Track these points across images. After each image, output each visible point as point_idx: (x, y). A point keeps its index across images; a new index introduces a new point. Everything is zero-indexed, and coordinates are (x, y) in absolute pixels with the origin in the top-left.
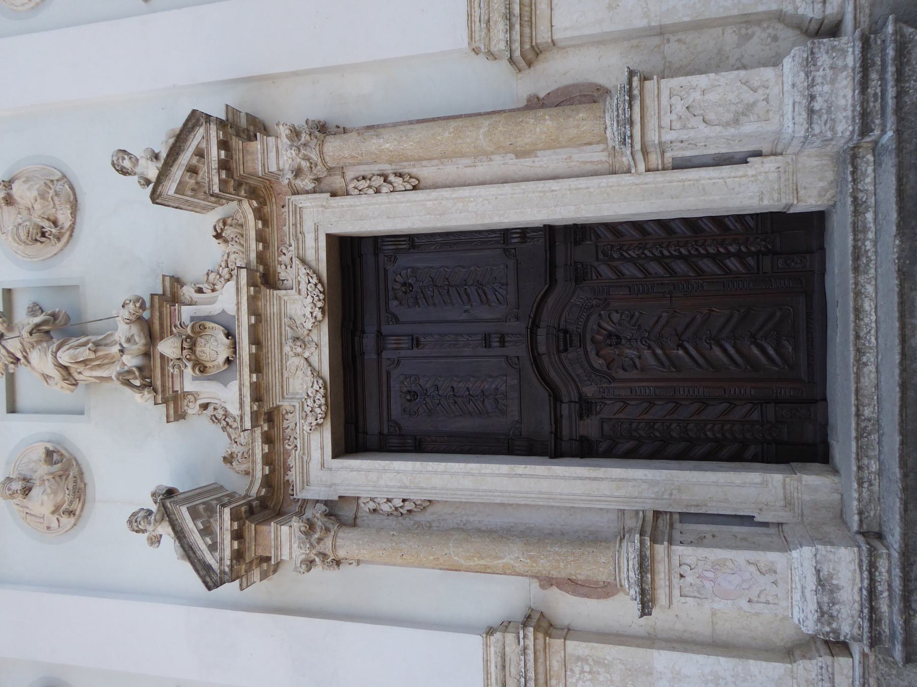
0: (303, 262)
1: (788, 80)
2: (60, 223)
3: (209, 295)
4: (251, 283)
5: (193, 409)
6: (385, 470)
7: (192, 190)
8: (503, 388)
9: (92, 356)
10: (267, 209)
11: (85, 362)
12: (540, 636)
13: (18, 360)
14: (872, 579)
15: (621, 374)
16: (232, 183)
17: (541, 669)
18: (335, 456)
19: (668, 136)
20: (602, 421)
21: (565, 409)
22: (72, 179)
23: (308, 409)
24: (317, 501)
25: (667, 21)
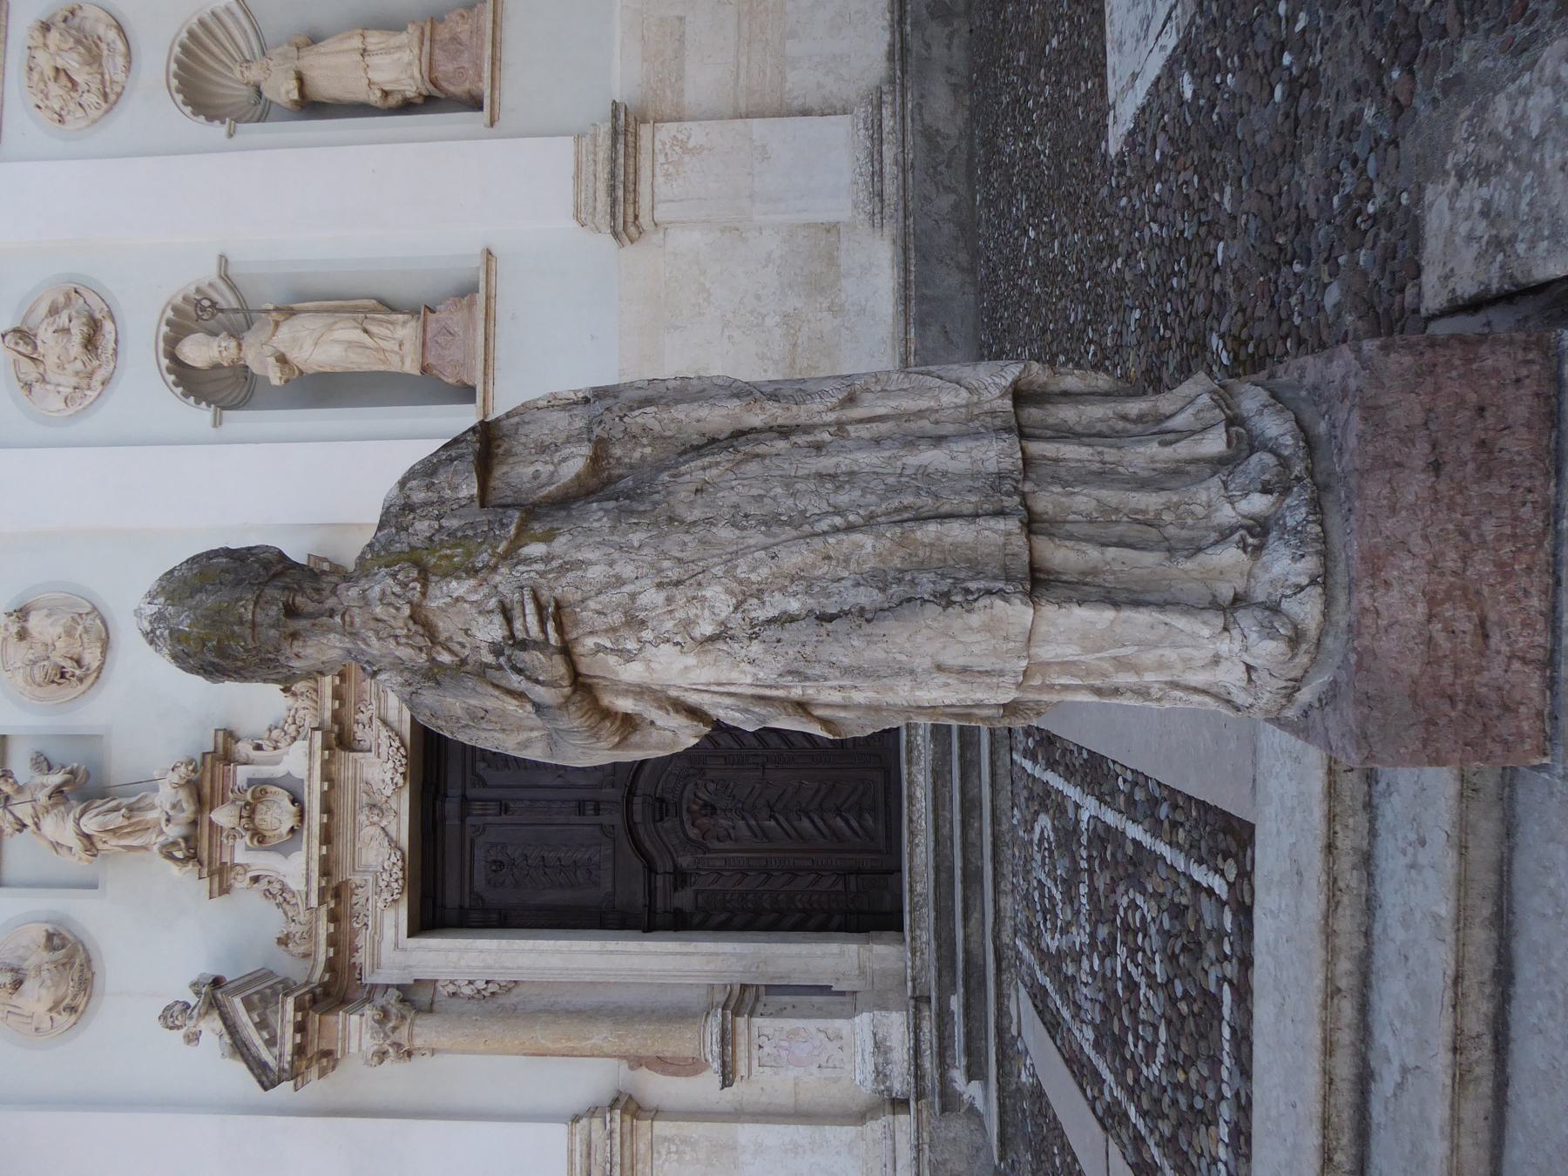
0: (385, 722)
3: (268, 753)
4: (326, 746)
5: (241, 882)
6: (467, 950)
8: (596, 859)
11: (114, 831)
12: (627, 1118)
13: (25, 826)
14: (917, 1040)
15: (716, 845)
17: (627, 1154)
18: (411, 934)
20: (697, 893)
21: (660, 881)
22: (106, 616)
23: (383, 884)
24: (388, 986)
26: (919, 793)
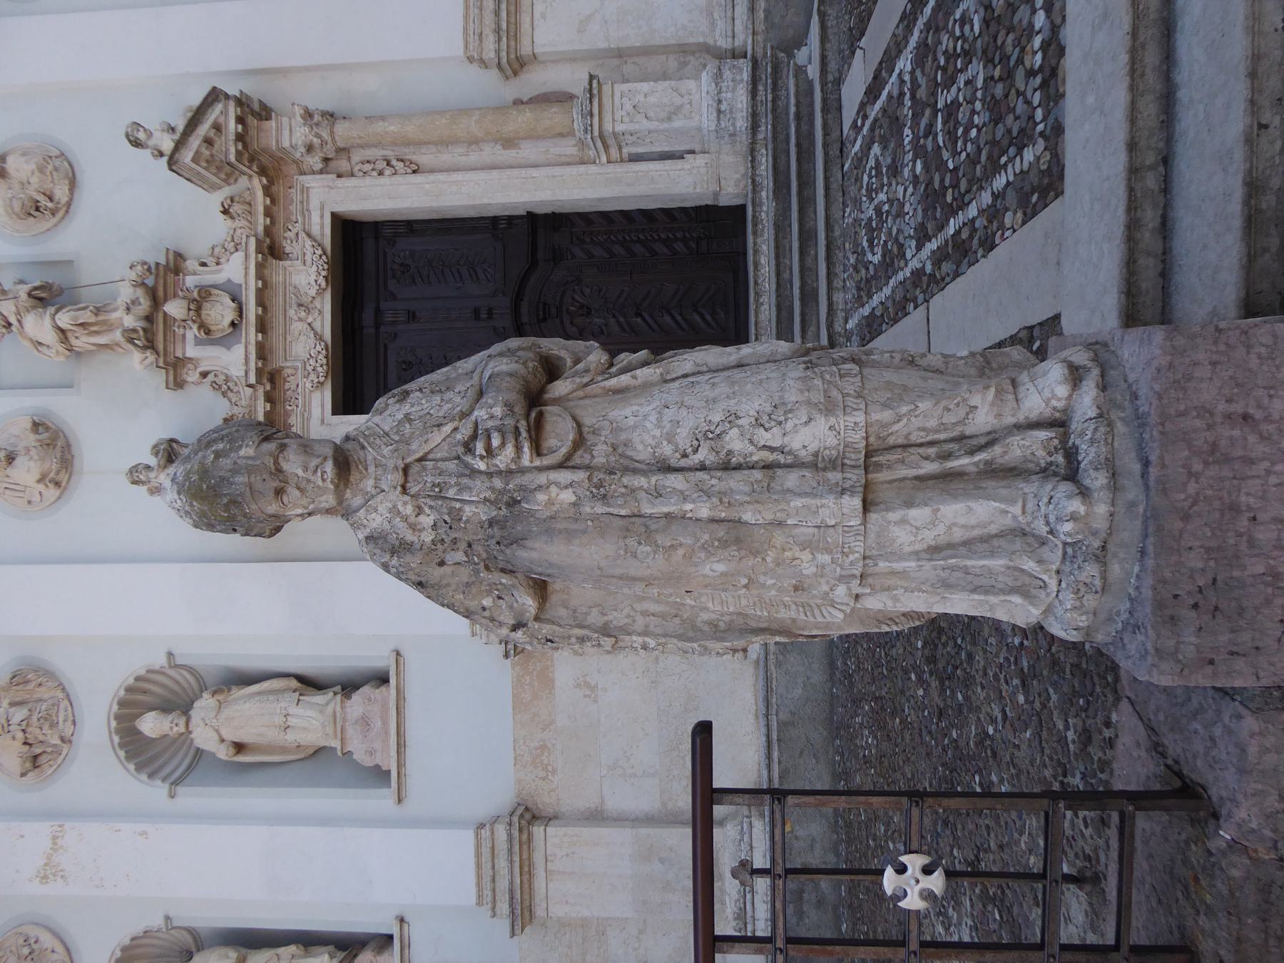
1: (705, 89)
2: (56, 198)
3: (213, 267)
5: (192, 377)
7: (207, 161)
9: (93, 319)
10: (274, 189)
11: (83, 325)
13: (10, 325)
16: (246, 155)
19: (620, 128)
22: (70, 157)
23: (310, 368)
25: (624, 45)
26: (763, 260)
